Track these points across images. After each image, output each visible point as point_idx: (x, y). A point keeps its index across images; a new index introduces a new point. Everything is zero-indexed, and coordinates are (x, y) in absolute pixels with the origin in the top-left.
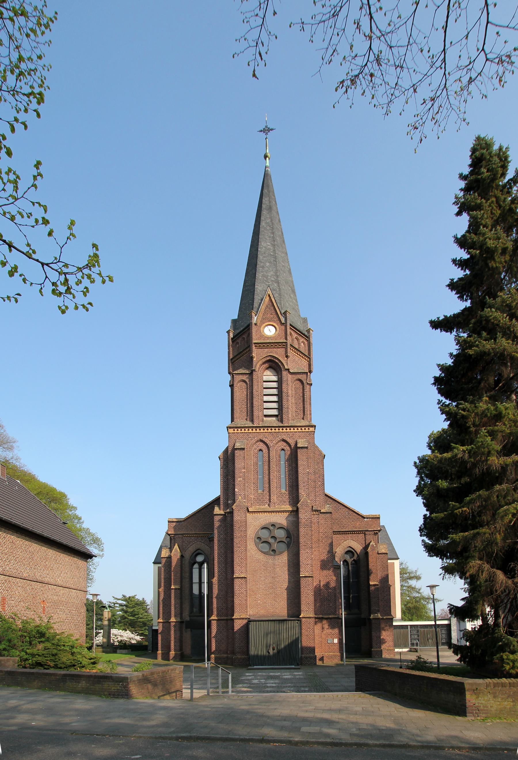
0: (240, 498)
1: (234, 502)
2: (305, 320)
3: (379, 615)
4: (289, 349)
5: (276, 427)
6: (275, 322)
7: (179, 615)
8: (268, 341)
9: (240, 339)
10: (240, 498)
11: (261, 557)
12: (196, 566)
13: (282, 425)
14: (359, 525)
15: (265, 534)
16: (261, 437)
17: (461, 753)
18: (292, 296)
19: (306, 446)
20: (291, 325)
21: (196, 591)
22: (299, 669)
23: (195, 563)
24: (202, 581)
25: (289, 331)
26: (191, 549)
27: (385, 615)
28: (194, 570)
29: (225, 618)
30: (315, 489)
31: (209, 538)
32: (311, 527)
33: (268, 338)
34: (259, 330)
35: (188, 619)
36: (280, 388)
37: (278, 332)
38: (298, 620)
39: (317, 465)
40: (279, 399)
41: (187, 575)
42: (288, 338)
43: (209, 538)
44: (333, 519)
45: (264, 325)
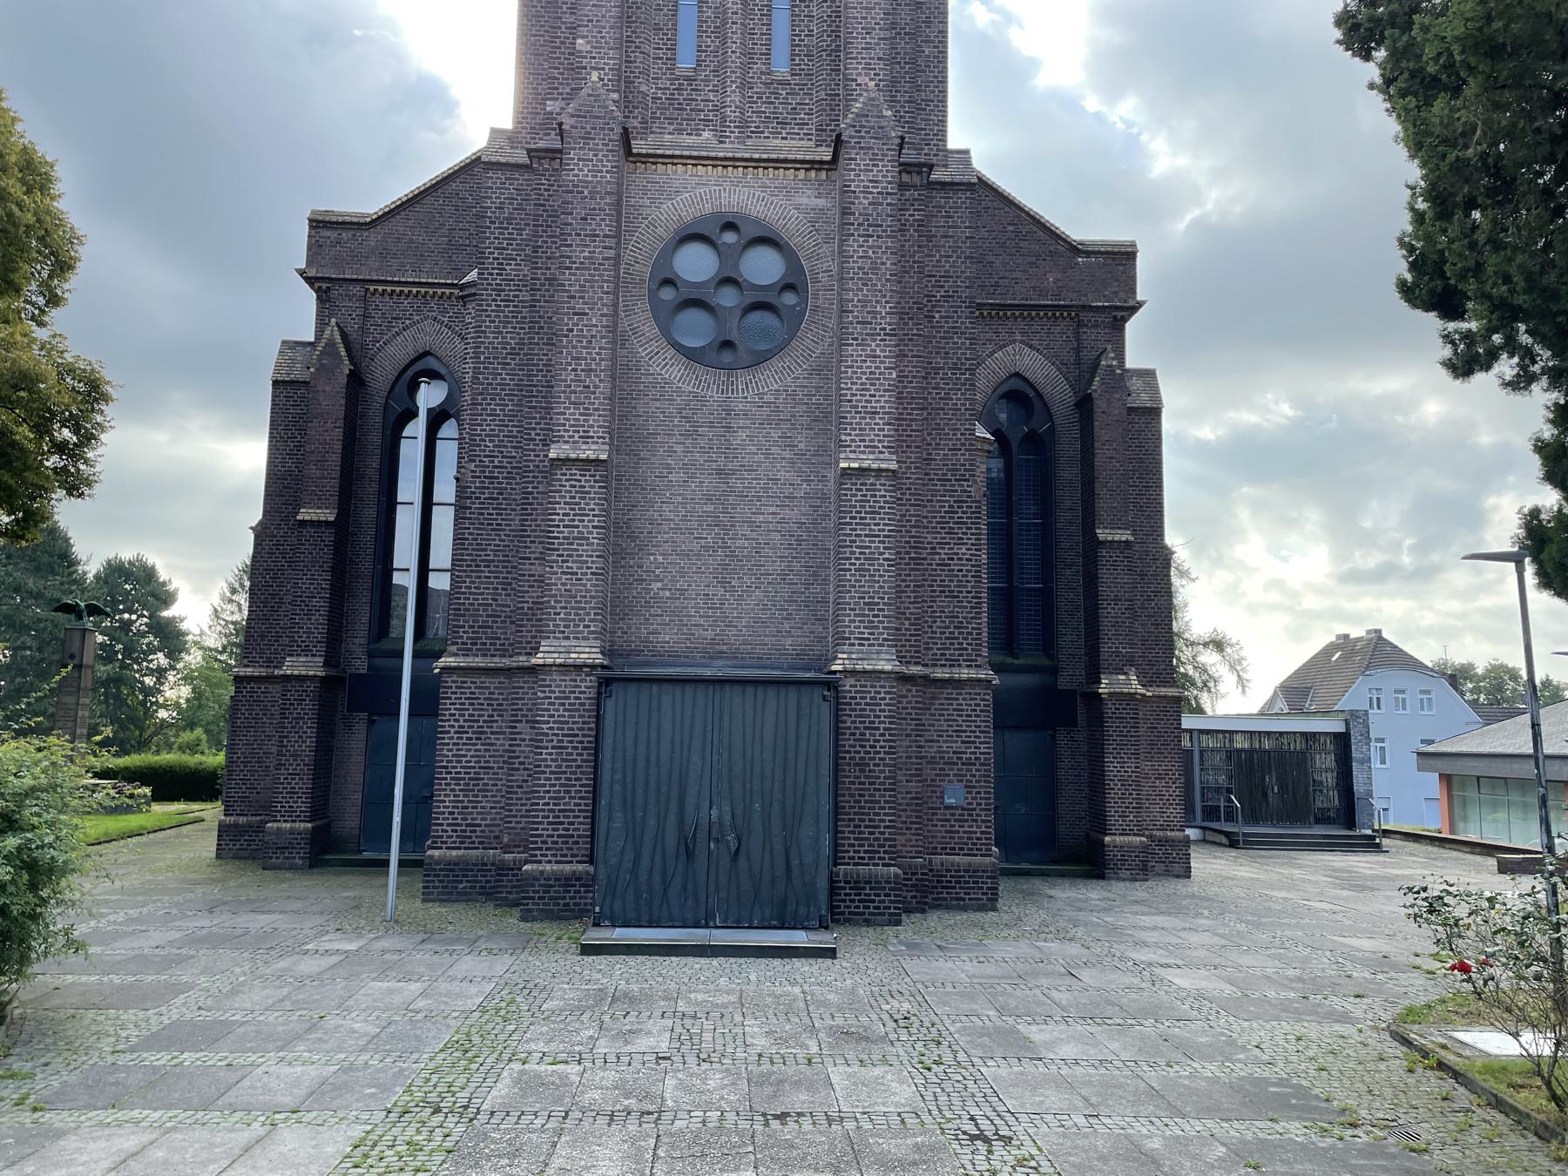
0: (595, 76)
7: (322, 648)
17: (990, 969)
22: (831, 953)
28: (405, 446)
41: (373, 463)
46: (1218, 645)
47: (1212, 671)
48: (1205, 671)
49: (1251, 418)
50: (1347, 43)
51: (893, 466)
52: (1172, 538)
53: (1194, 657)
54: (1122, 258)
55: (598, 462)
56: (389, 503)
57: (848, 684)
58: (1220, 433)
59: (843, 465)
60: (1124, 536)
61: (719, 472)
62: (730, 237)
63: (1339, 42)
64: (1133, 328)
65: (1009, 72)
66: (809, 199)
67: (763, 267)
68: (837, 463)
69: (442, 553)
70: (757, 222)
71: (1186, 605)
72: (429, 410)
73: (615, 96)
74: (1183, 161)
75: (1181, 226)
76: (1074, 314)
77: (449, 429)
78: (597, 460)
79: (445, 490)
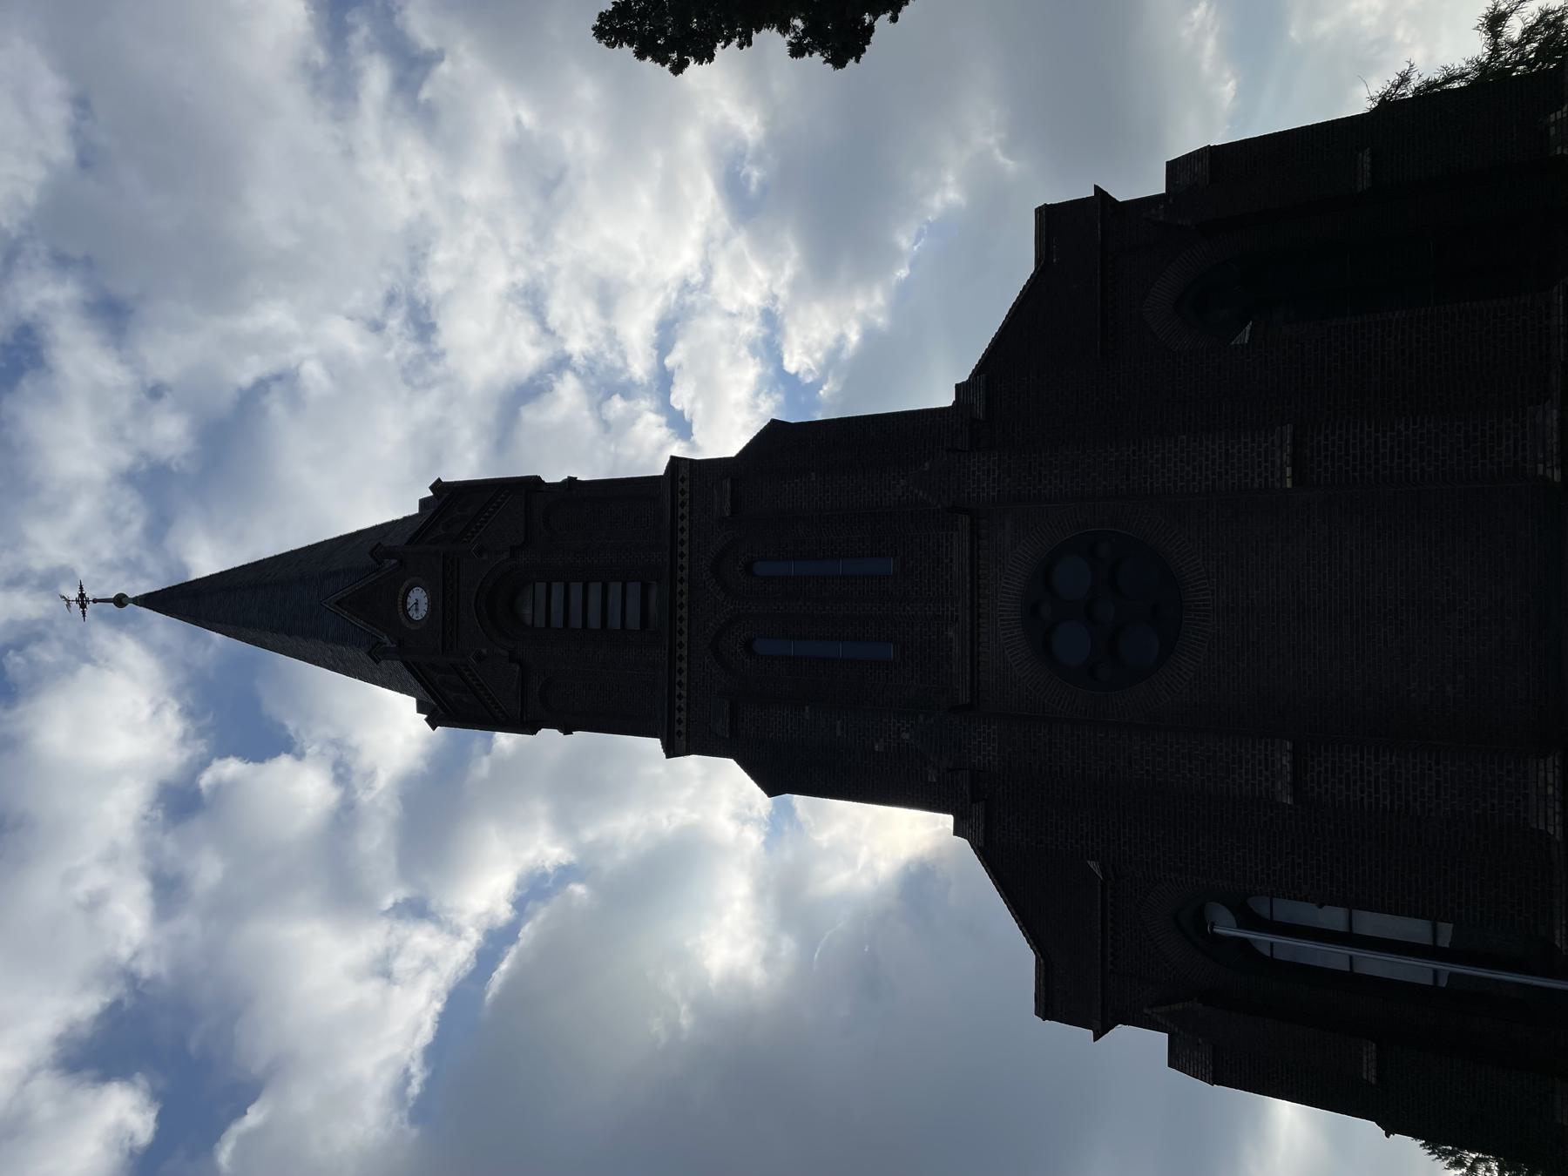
0: (906, 736)
28: (1281, 955)
46: (1495, 22)
47: (1531, 20)
48: (1532, 28)
49: (1210, 44)
50: (857, 52)
51: (1289, 429)
52: (1359, 101)
53: (1513, 45)
54: (1051, 220)
56: (1351, 980)
58: (1227, 75)
63: (857, 61)
64: (1122, 192)
65: (878, 351)
69: (1415, 929)
71: (1445, 68)
72: (1239, 927)
73: (921, 718)
74: (950, 178)
75: (1010, 165)
77: (1261, 907)
79: (1333, 917)
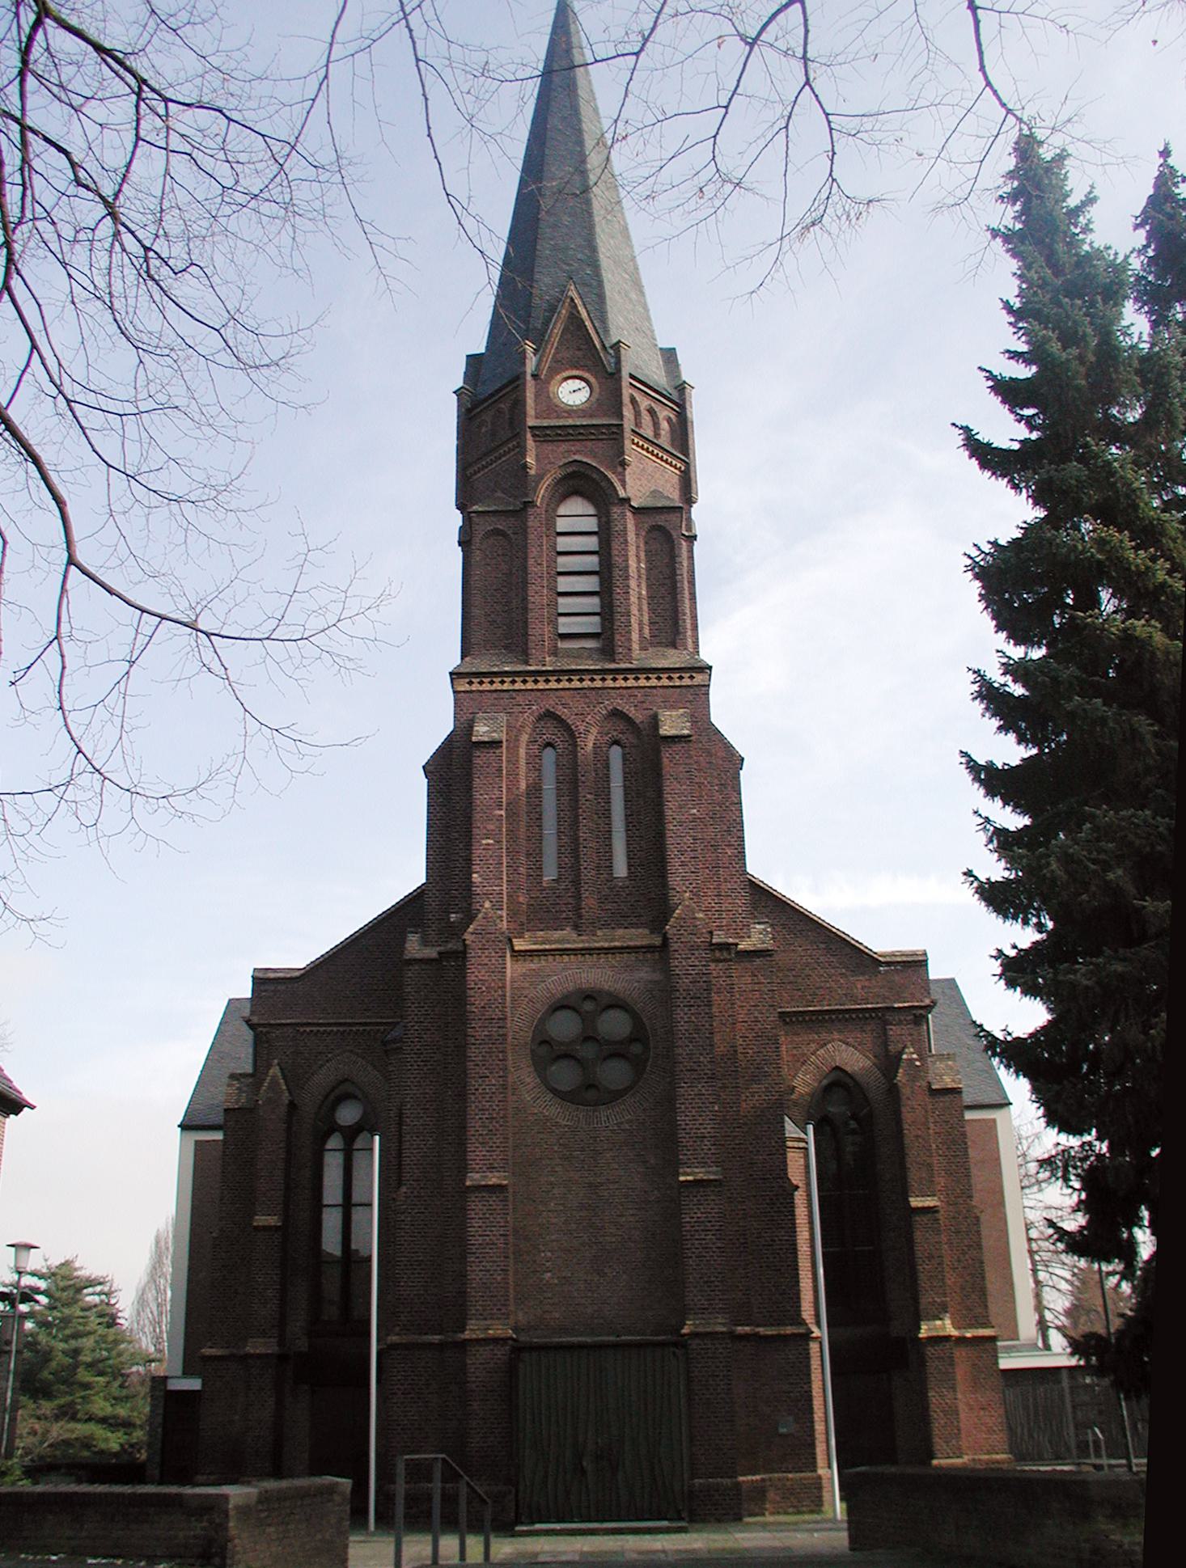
0: (487, 905)
1: (470, 917)
2: (670, 356)
3: (948, 1322)
4: (627, 443)
5: (595, 672)
6: (589, 371)
8: (570, 422)
9: (491, 413)
10: (487, 905)
11: (553, 1109)
12: (335, 1142)
13: (613, 666)
14: (863, 993)
15: (565, 1027)
16: (550, 703)
18: (633, 296)
19: (686, 732)
20: (632, 377)
21: (331, 1242)
23: (333, 1128)
24: (356, 1197)
25: (627, 392)
26: (323, 1078)
27: (971, 1326)
29: (436, 1338)
30: (717, 874)
31: (384, 1043)
32: (709, 1005)
33: (571, 411)
34: (543, 394)
35: (302, 1344)
36: (604, 552)
37: (596, 395)
38: (676, 1344)
39: (720, 791)
40: (601, 584)
42: (625, 413)
43: (384, 1043)
44: (780, 970)
45: (559, 377)
55: (501, 1188)
56: (317, 1205)
57: (694, 1343)
59: (682, 1178)
60: (929, 1202)
61: (590, 1185)
62: (588, 1006)
66: (645, 974)
67: (614, 1025)
68: (678, 1174)
70: (609, 994)
76: (878, 1019)
78: (500, 1186)
